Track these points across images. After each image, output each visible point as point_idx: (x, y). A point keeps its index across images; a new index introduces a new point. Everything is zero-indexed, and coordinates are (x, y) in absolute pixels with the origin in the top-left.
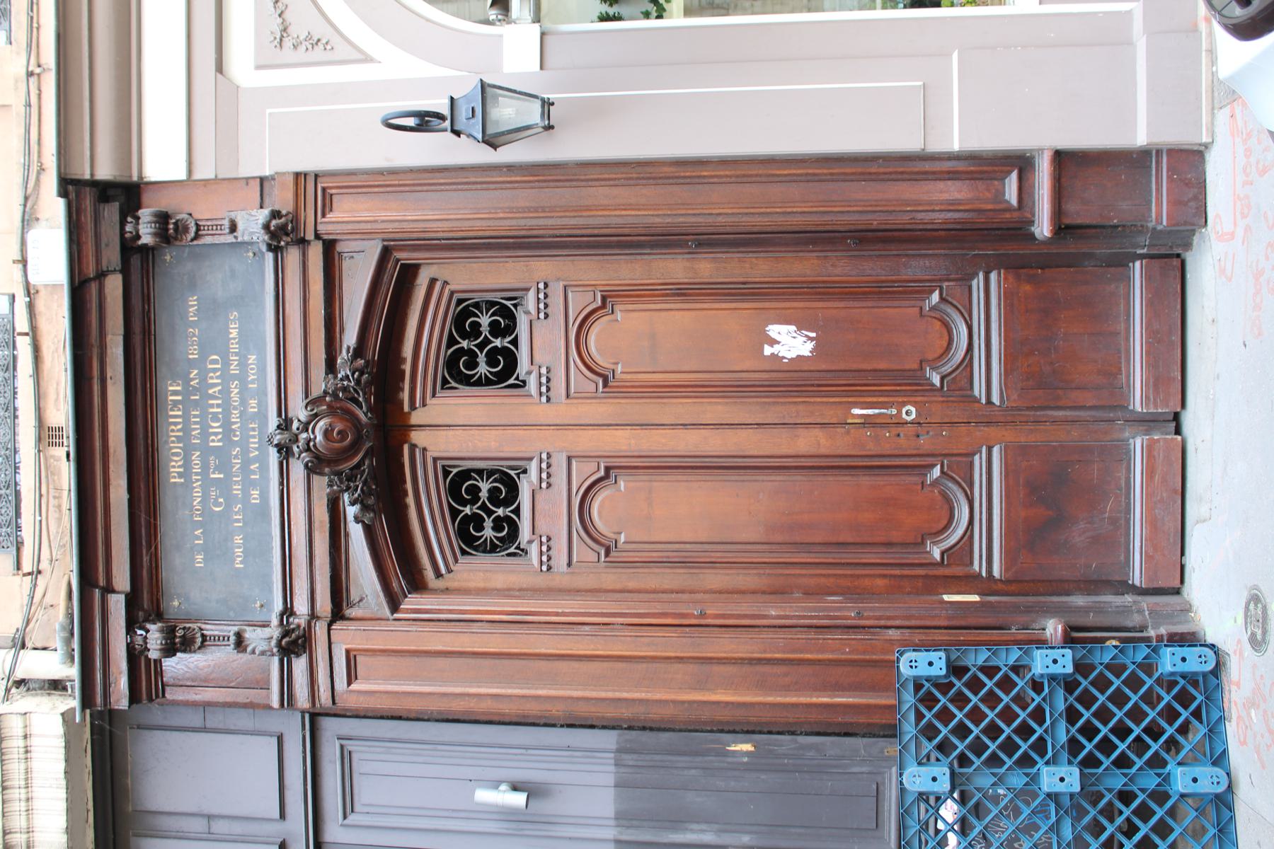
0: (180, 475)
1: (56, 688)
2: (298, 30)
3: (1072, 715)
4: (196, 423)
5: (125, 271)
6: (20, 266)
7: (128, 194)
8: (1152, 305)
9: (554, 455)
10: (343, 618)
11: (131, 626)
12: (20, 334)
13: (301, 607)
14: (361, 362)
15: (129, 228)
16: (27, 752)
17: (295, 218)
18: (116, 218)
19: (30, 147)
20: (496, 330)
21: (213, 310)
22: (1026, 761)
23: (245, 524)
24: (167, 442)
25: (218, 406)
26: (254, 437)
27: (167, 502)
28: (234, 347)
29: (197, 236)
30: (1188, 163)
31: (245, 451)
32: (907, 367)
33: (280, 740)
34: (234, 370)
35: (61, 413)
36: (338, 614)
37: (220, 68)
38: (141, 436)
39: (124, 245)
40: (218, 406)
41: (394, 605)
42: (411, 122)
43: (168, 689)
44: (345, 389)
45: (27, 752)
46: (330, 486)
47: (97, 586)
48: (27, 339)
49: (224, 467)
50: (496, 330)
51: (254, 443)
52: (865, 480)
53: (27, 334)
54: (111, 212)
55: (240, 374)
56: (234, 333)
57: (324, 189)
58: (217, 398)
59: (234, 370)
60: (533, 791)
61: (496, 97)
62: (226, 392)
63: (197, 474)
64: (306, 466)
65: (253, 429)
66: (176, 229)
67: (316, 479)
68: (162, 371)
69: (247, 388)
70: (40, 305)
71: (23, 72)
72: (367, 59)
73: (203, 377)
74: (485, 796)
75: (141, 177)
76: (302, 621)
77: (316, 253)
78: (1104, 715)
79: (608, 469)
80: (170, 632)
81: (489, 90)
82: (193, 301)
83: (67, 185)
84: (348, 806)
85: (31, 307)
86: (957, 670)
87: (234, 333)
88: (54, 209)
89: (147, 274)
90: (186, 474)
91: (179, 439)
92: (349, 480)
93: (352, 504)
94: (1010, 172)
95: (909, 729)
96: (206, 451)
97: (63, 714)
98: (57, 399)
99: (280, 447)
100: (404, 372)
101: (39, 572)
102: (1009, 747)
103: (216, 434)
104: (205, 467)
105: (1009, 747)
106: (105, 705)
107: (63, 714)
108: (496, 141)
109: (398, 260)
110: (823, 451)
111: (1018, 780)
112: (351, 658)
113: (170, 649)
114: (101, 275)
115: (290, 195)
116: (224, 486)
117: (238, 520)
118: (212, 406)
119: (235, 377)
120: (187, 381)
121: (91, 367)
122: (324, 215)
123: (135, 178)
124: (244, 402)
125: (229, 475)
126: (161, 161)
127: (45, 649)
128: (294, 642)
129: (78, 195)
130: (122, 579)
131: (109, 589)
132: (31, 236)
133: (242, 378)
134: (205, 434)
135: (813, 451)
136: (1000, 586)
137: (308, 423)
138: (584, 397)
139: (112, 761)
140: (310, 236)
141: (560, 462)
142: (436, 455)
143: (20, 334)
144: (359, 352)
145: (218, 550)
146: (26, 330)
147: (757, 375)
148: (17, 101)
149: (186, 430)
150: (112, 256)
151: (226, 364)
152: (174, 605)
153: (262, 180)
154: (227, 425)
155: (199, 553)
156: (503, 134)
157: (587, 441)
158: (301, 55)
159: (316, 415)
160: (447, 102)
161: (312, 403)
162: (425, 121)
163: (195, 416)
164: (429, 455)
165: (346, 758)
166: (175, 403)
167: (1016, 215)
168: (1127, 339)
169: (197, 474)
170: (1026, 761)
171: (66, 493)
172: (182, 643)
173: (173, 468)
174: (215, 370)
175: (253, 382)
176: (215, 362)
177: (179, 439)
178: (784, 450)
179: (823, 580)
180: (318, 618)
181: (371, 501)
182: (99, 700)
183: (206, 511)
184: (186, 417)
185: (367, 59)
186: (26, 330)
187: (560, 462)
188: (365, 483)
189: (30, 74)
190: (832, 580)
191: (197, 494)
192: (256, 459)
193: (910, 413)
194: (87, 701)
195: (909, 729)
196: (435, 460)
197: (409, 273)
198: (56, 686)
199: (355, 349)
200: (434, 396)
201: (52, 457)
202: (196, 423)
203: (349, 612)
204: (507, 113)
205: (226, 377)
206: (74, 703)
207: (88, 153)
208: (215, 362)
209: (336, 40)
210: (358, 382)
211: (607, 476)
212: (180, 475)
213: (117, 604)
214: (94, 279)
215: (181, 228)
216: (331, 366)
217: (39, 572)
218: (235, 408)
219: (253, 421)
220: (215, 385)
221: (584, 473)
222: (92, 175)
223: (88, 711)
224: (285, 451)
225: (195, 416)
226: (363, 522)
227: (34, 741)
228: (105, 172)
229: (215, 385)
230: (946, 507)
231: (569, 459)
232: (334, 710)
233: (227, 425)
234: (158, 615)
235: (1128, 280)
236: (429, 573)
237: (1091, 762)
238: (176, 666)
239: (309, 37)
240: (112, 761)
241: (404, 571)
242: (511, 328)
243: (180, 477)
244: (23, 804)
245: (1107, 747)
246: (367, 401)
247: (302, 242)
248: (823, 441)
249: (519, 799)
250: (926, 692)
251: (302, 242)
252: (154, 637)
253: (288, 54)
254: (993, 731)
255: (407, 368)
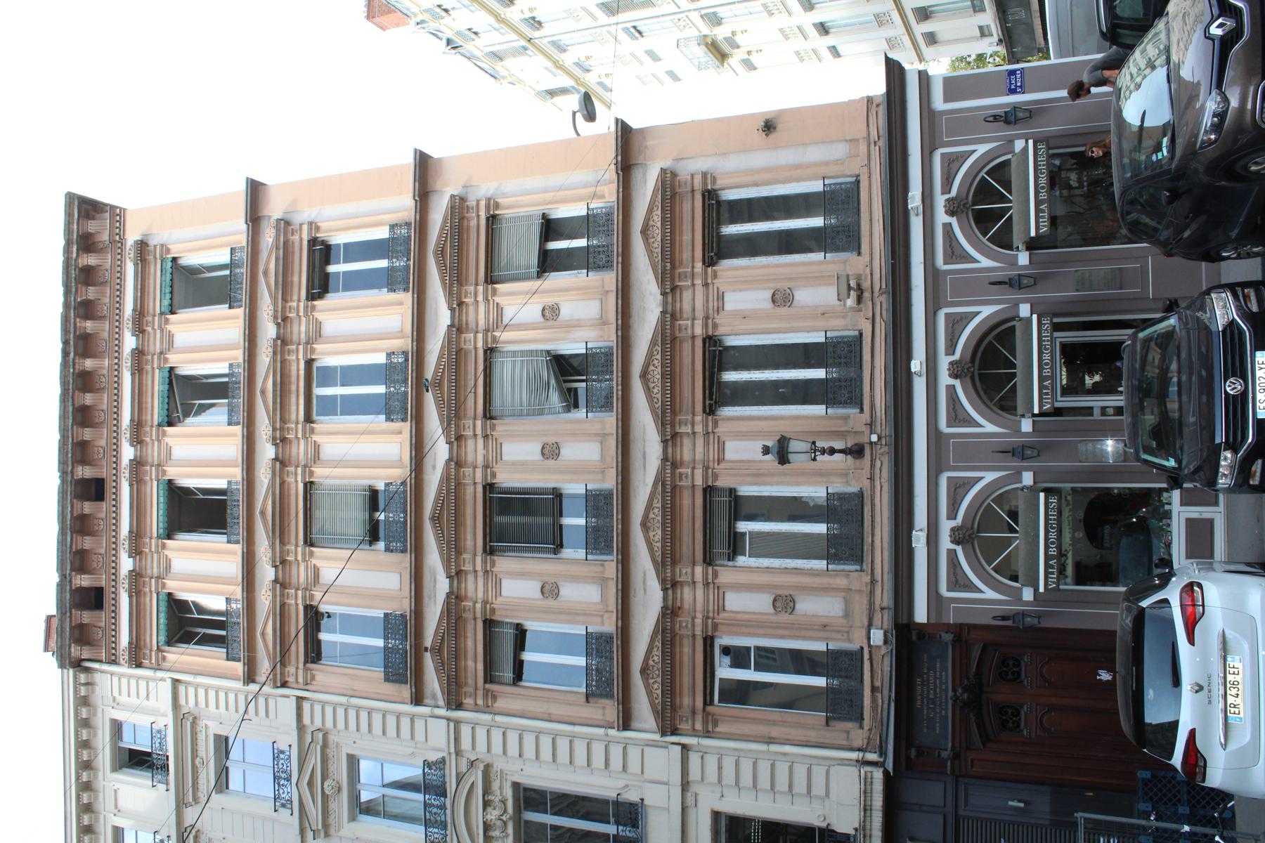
3: (1189, 792)
20: (1014, 665)
22: (1175, 805)
50: (1014, 665)
60: (1026, 803)
74: (1011, 803)
78: (1165, 786)
84: (966, 804)
85: (870, 652)
86: (1154, 776)
95: (1140, 792)
102: (1170, 800)
105: (1170, 800)
111: (1172, 809)
112: (972, 762)
116: (934, 709)
165: (966, 790)
170: (1175, 805)
195: (1140, 792)
205: (935, 678)
232: (828, 763)
237: (1194, 806)
242: (1019, 664)
245: (1199, 802)
249: (1022, 805)
250: (1146, 782)
252: (913, 753)
254: (1165, 795)
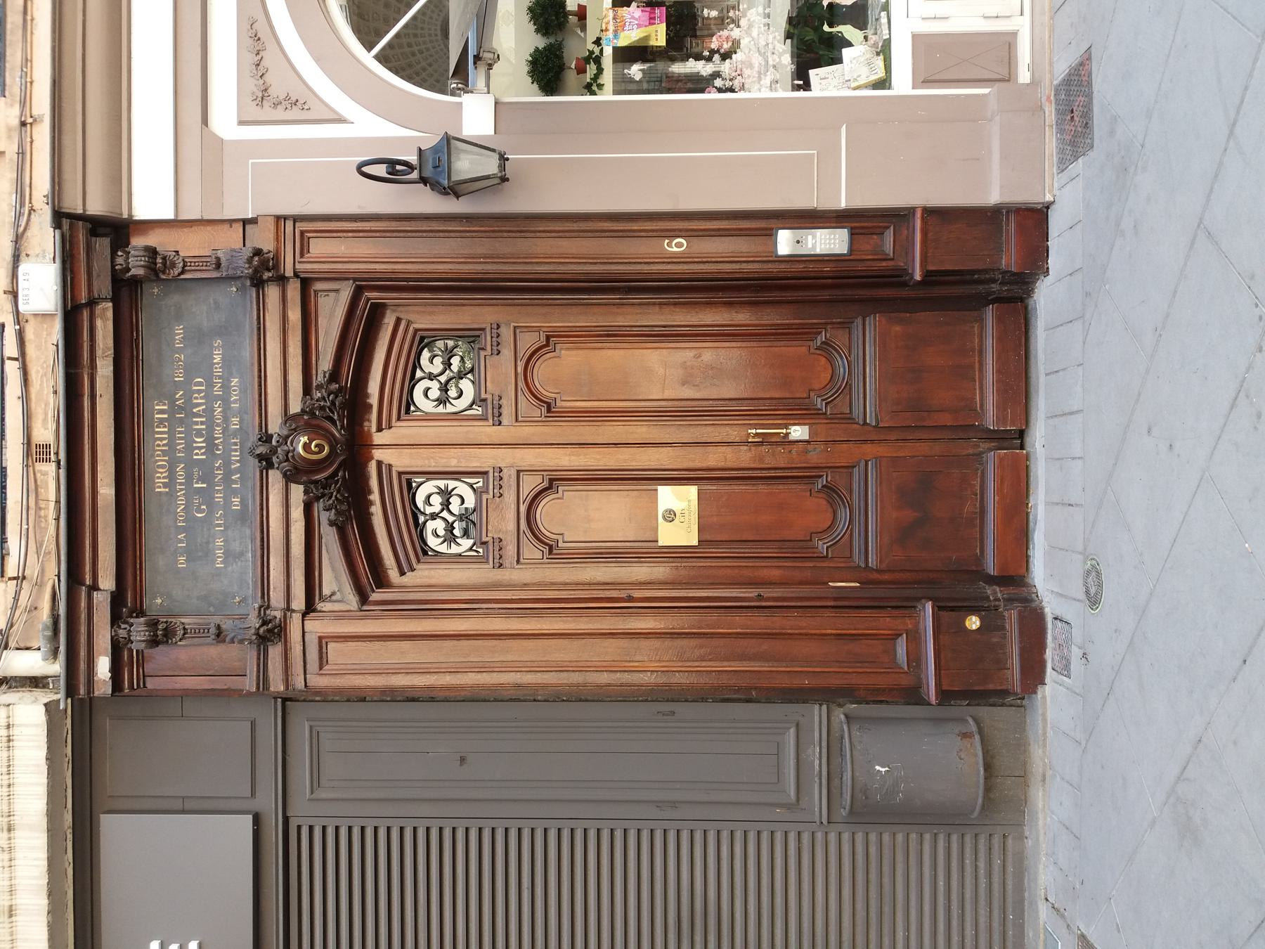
0: (165, 485)
1: (36, 687)
2: (276, 91)
4: (180, 438)
5: (116, 300)
6: (10, 297)
7: (117, 230)
8: (1001, 339)
9: (505, 471)
10: (314, 611)
11: (116, 619)
12: (10, 358)
13: (277, 598)
14: (335, 386)
15: (120, 260)
16: (9, 741)
17: (276, 257)
18: (108, 251)
19: (22, 189)
21: (199, 338)
23: (226, 528)
24: (153, 456)
25: (202, 423)
26: (236, 450)
27: (151, 508)
28: (218, 371)
29: (182, 272)
30: (1034, 220)
31: (227, 463)
32: (798, 395)
33: (253, 724)
34: (217, 391)
35: (48, 431)
36: (310, 608)
37: (205, 121)
38: (129, 449)
39: (115, 274)
40: (202, 423)
41: (363, 598)
42: (381, 170)
43: (148, 679)
44: (322, 408)
45: (9, 741)
46: (306, 492)
47: (84, 584)
48: (16, 364)
49: (207, 477)
51: (235, 456)
52: (762, 488)
53: (16, 359)
54: (103, 245)
55: (226, 386)
56: (217, 359)
57: (302, 233)
58: (201, 416)
59: (217, 391)
61: (459, 151)
62: (209, 411)
63: (181, 484)
64: (285, 475)
65: (235, 444)
66: (164, 264)
67: (293, 486)
68: (149, 392)
69: (229, 408)
70: (30, 335)
71: (16, 122)
72: (341, 120)
73: (188, 396)
75: (130, 215)
76: (278, 614)
77: (294, 290)
79: (551, 481)
80: (153, 625)
81: (454, 142)
82: (179, 330)
83: (59, 217)
85: (21, 336)
87: (217, 359)
88: (43, 237)
89: (135, 306)
90: (171, 483)
91: (164, 453)
92: (324, 488)
93: (327, 509)
94: (888, 227)
96: (190, 464)
97: (46, 705)
98: (45, 420)
99: (261, 457)
100: (371, 406)
101: (24, 578)
103: (200, 448)
104: (189, 478)
106: (89, 693)
107: (46, 705)
108: (458, 188)
109: (369, 299)
110: (729, 465)
113: (154, 642)
114: (92, 303)
115: (271, 236)
116: (207, 495)
117: (219, 525)
118: (197, 423)
119: (218, 398)
120: (172, 401)
121: (83, 385)
122: (302, 255)
123: (125, 216)
124: (226, 419)
125: (211, 485)
126: (151, 198)
127: (27, 649)
128: (269, 631)
129: (71, 227)
130: (107, 582)
131: (94, 587)
132: (22, 269)
133: (225, 400)
134: (189, 448)
135: (721, 464)
136: (876, 576)
137: (288, 437)
138: (530, 421)
139: (912, 719)
140: (289, 273)
141: (509, 475)
142: (401, 470)
143: (10, 358)
144: (334, 375)
145: (198, 553)
146: (15, 354)
147: (670, 403)
148: (12, 149)
149: (172, 444)
150: (103, 286)
151: (210, 385)
152: (155, 602)
153: (245, 222)
154: (210, 441)
155: (182, 555)
156: (465, 182)
157: (529, 458)
158: (279, 114)
159: (295, 430)
160: (416, 152)
161: (288, 418)
162: (395, 171)
163: (180, 432)
164: (394, 469)
165: (315, 737)
166: (161, 421)
167: (891, 263)
168: (981, 371)
169: (181, 484)
171: (52, 505)
172: (165, 635)
173: (158, 478)
174: (199, 391)
175: (235, 401)
176: (200, 384)
177: (164, 453)
178: (697, 465)
179: (729, 571)
180: (293, 611)
181: (344, 507)
182: (82, 691)
183: (189, 519)
184: (171, 433)
185: (341, 120)
186: (15, 354)
187: (509, 475)
188: (338, 491)
189: (23, 124)
190: (737, 571)
191: (181, 501)
192: (237, 471)
193: (798, 432)
194: (71, 691)
196: (400, 474)
197: (377, 312)
198: (35, 682)
199: (331, 375)
200: (399, 419)
201: (40, 471)
202: (180, 438)
203: (320, 606)
204: (466, 166)
205: (210, 398)
206: (60, 696)
207: (80, 64)
208: (200, 384)
209: (311, 102)
210: (333, 403)
211: (550, 487)
212: (165, 485)
213: (102, 601)
214: (86, 305)
215: (168, 264)
216: (307, 390)
217: (24, 578)
218: (218, 425)
219: (235, 437)
220: (199, 405)
221: (530, 484)
222: (84, 210)
223: (69, 700)
224: (266, 462)
225: (180, 432)
226: (336, 525)
227: (15, 731)
228: (96, 207)
229: (199, 405)
230: (830, 510)
231: (518, 472)
233: (210, 441)
234: (141, 613)
235: (981, 321)
236: (393, 574)
238: (161, 657)
239: (287, 98)
240: (912, 719)
241: (369, 575)
243: (165, 487)
244: (5, 789)
246: (341, 418)
247: (281, 280)
248: (729, 456)
251: (281, 280)
252: (138, 632)
253: (268, 112)
255: (374, 401)
